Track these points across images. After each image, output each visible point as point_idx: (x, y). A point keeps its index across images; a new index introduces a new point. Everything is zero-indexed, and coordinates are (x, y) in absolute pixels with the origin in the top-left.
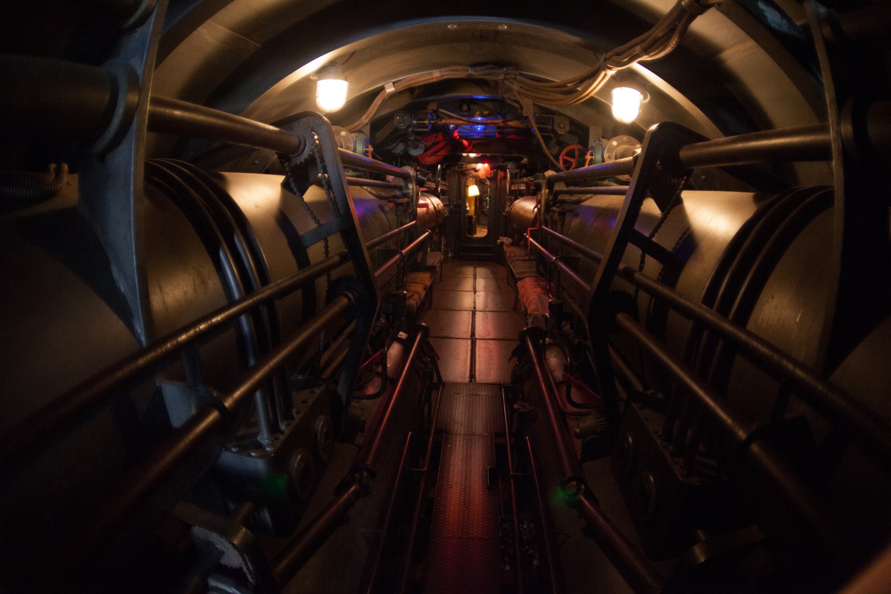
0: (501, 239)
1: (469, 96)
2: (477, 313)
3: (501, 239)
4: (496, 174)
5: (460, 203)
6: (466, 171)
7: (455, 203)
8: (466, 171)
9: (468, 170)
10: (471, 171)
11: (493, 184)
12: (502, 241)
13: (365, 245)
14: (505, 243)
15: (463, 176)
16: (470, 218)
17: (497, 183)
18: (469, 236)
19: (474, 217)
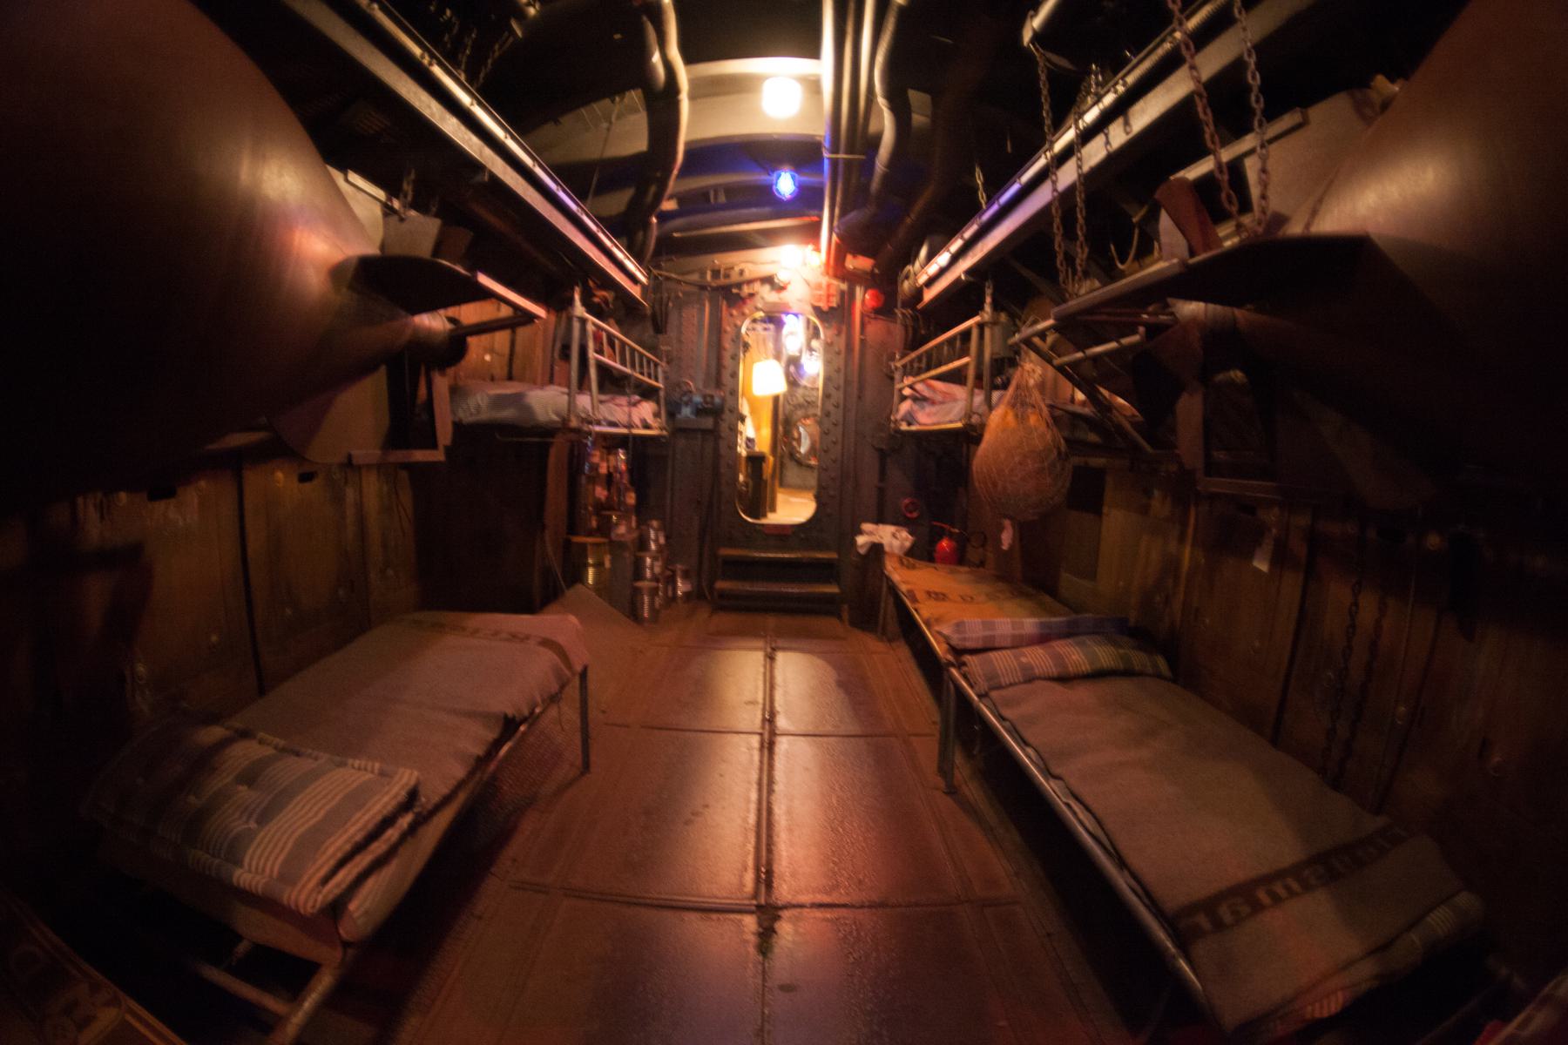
0: (870, 533)
1: (347, 842)
2: (783, 745)
3: (870, 533)
4: (847, 299)
5: (717, 400)
6: (739, 285)
7: (698, 399)
8: (739, 285)
9: (750, 282)
10: (757, 287)
11: (839, 334)
12: (876, 539)
13: (683, 137)
14: (887, 549)
15: (730, 306)
16: (756, 460)
17: (850, 325)
18: (749, 520)
19: (771, 459)
